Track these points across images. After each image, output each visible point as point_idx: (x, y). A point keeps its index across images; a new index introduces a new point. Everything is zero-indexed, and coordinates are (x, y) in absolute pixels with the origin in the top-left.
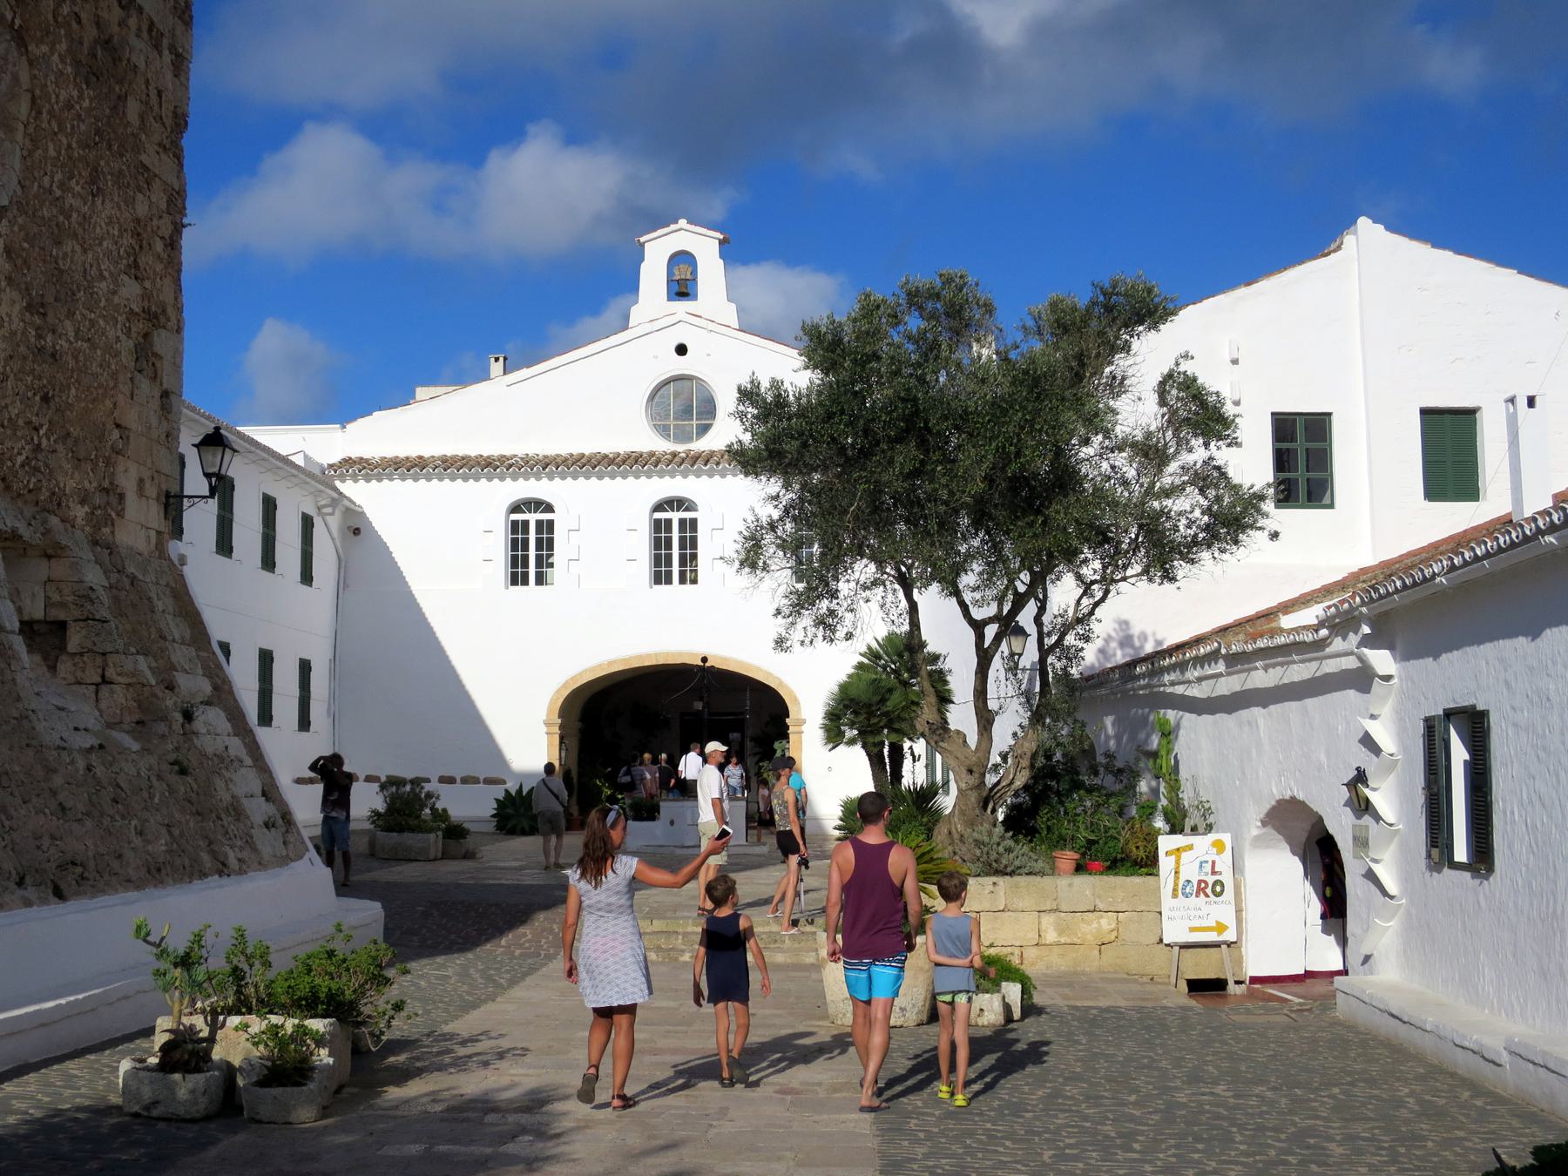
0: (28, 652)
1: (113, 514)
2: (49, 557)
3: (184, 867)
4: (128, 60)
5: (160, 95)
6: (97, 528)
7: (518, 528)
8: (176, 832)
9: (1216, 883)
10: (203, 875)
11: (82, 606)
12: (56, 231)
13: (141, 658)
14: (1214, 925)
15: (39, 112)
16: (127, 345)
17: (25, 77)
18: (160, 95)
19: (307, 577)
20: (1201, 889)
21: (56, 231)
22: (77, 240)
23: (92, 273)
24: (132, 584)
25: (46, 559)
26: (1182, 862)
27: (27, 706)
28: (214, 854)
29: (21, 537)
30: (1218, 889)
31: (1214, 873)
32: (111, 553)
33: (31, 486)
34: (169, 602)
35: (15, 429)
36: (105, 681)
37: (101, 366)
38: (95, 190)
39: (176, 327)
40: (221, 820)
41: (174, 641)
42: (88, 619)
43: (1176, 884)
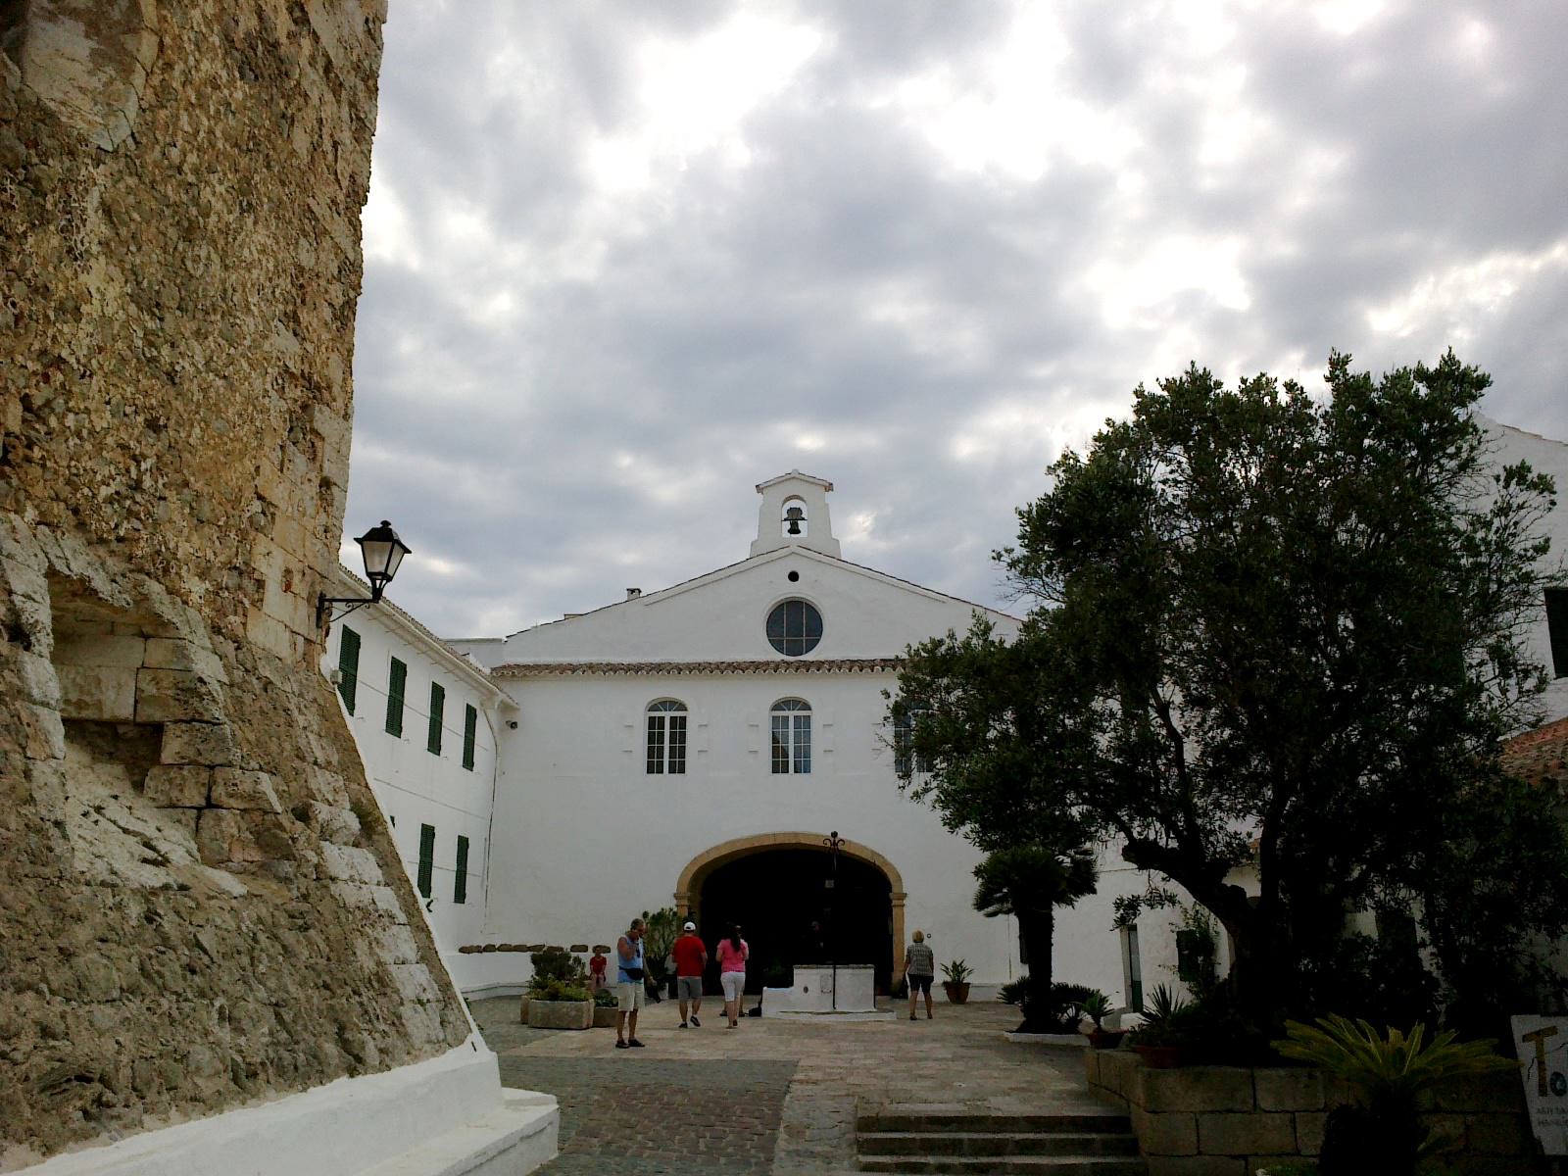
0: (66, 736)
1: (246, 602)
2: (146, 637)
3: (296, 1068)
4: (299, 83)
5: (335, 145)
6: (221, 612)
7: (655, 724)
8: (287, 1017)
11: (186, 702)
13: (264, 776)
15: (169, 66)
16: (277, 405)
19: (468, 762)
22: (216, 248)
23: (235, 299)
27: (44, 812)
28: (344, 1044)
29: (96, 592)
30: (1558, 1085)
32: (238, 648)
33: (122, 533)
35: (100, 447)
36: (211, 804)
38: (244, 198)
39: (343, 412)
40: (360, 995)
41: (315, 763)
42: (193, 720)
43: (1542, 1078)
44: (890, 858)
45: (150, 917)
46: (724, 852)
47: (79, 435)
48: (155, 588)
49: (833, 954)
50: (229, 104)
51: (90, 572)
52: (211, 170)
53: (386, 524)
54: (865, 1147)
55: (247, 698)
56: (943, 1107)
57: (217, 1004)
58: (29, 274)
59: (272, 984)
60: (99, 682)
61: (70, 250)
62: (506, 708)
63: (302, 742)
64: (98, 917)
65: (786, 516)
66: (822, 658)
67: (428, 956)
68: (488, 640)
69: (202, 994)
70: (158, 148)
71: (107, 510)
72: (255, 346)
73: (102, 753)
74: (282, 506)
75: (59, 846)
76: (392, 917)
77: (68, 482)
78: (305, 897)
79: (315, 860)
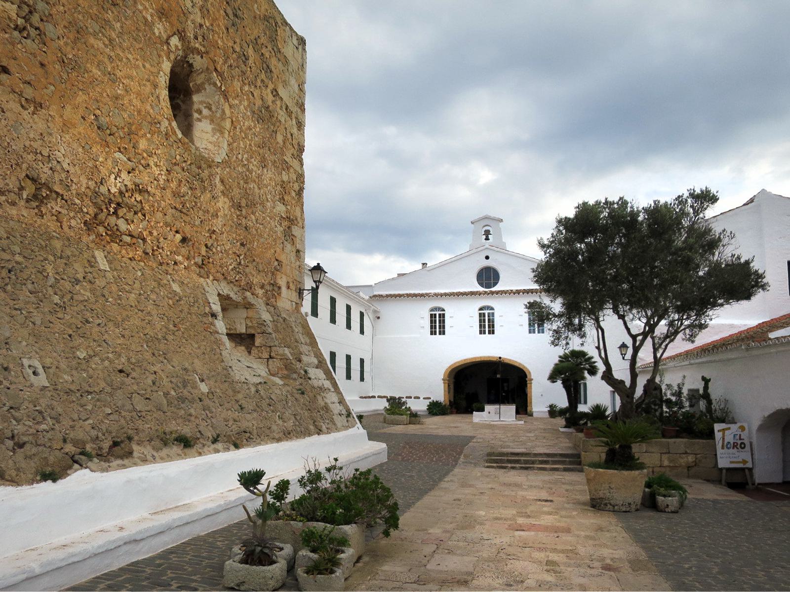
1: (276, 294)
2: (247, 308)
4: (277, 118)
5: (292, 135)
8: (298, 418)
9: (742, 443)
10: (310, 435)
12: (245, 178)
13: (286, 349)
14: (741, 460)
15: (235, 128)
16: (279, 229)
17: (228, 112)
18: (292, 135)
19: (362, 332)
20: (735, 446)
21: (245, 178)
22: (255, 183)
24: (284, 321)
25: (245, 309)
26: (726, 434)
27: (226, 364)
28: (316, 426)
30: (743, 446)
31: (740, 439)
32: (275, 309)
33: (237, 279)
34: (300, 329)
35: (228, 254)
36: (271, 357)
37: (268, 236)
38: (263, 164)
41: (302, 343)
42: (263, 333)
44: (526, 365)
47: (222, 253)
49: (499, 399)
50: (255, 134)
51: (229, 293)
52: (252, 158)
53: (318, 264)
54: (487, 461)
55: (279, 325)
56: (518, 450)
57: (278, 414)
58: (203, 208)
59: (293, 409)
60: (235, 322)
61: (213, 197)
62: (375, 312)
63: (297, 337)
64: (244, 392)
66: (499, 289)
67: (342, 401)
69: (273, 411)
70: (235, 156)
71: (232, 273)
72: (271, 211)
73: (238, 343)
75: (232, 374)
76: (329, 390)
77: (220, 266)
78: (301, 384)
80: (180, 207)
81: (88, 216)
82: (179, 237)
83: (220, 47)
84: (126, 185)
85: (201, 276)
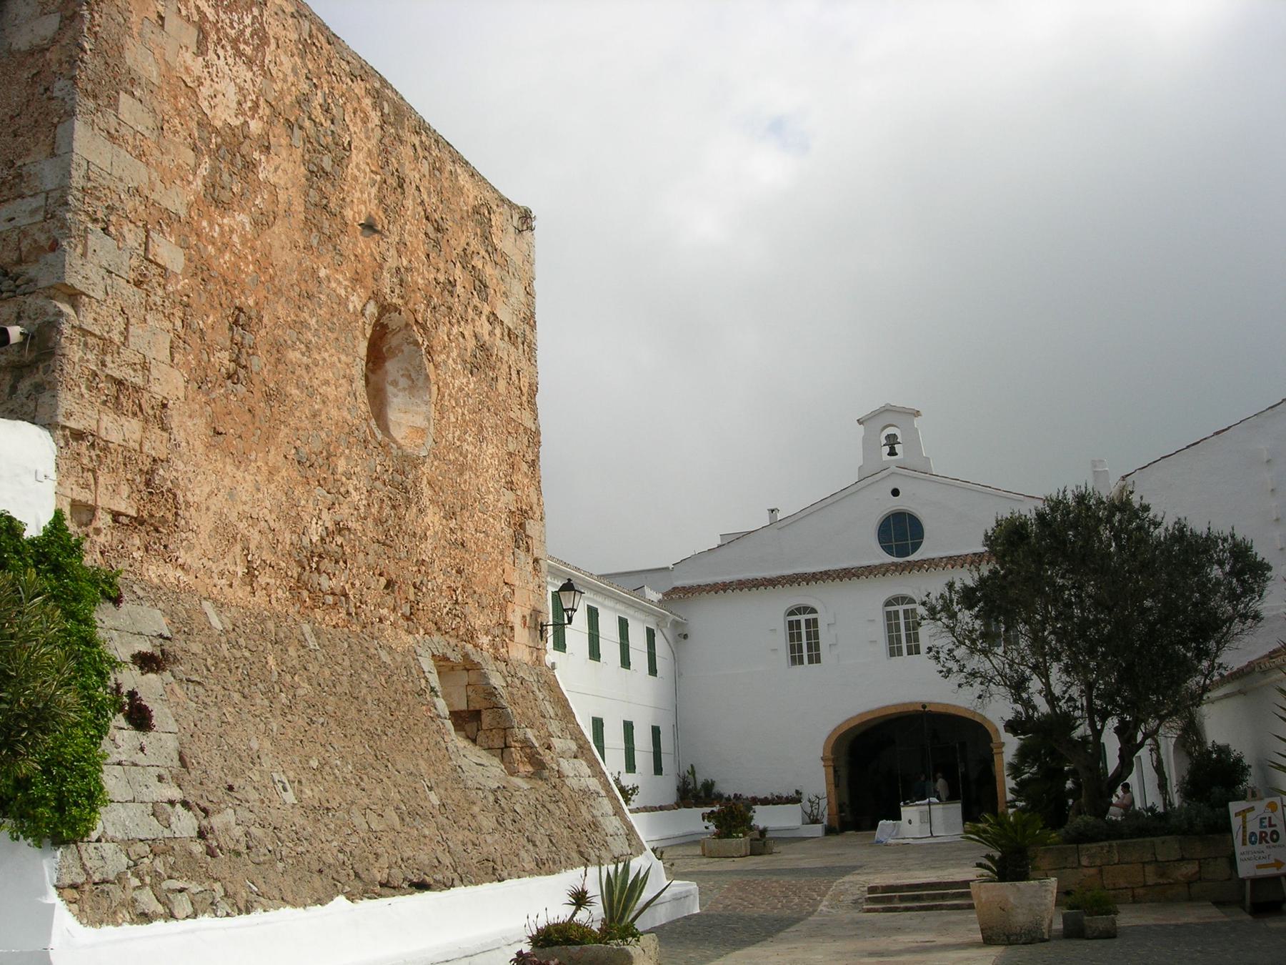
1: (507, 639)
4: (497, 355)
7: (793, 626)
9: (1274, 832)
13: (528, 730)
19: (653, 671)
20: (1262, 838)
25: (465, 672)
28: (581, 853)
30: (1275, 837)
31: (1271, 825)
36: (506, 747)
42: (493, 707)
43: (1244, 836)
45: (496, 801)
46: (877, 715)
48: (469, 647)
63: (542, 708)
65: (884, 442)
66: (924, 557)
68: (659, 569)
74: (517, 583)
76: (598, 793)
79: (557, 768)
80: (382, 538)
81: (292, 580)
82: (383, 581)
83: (420, 287)
84: (326, 528)
85: (410, 633)
